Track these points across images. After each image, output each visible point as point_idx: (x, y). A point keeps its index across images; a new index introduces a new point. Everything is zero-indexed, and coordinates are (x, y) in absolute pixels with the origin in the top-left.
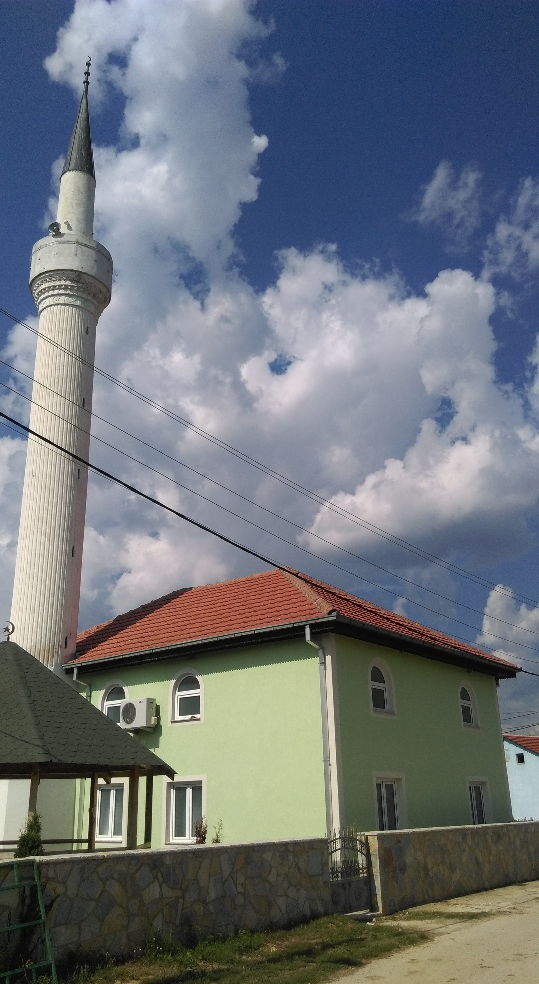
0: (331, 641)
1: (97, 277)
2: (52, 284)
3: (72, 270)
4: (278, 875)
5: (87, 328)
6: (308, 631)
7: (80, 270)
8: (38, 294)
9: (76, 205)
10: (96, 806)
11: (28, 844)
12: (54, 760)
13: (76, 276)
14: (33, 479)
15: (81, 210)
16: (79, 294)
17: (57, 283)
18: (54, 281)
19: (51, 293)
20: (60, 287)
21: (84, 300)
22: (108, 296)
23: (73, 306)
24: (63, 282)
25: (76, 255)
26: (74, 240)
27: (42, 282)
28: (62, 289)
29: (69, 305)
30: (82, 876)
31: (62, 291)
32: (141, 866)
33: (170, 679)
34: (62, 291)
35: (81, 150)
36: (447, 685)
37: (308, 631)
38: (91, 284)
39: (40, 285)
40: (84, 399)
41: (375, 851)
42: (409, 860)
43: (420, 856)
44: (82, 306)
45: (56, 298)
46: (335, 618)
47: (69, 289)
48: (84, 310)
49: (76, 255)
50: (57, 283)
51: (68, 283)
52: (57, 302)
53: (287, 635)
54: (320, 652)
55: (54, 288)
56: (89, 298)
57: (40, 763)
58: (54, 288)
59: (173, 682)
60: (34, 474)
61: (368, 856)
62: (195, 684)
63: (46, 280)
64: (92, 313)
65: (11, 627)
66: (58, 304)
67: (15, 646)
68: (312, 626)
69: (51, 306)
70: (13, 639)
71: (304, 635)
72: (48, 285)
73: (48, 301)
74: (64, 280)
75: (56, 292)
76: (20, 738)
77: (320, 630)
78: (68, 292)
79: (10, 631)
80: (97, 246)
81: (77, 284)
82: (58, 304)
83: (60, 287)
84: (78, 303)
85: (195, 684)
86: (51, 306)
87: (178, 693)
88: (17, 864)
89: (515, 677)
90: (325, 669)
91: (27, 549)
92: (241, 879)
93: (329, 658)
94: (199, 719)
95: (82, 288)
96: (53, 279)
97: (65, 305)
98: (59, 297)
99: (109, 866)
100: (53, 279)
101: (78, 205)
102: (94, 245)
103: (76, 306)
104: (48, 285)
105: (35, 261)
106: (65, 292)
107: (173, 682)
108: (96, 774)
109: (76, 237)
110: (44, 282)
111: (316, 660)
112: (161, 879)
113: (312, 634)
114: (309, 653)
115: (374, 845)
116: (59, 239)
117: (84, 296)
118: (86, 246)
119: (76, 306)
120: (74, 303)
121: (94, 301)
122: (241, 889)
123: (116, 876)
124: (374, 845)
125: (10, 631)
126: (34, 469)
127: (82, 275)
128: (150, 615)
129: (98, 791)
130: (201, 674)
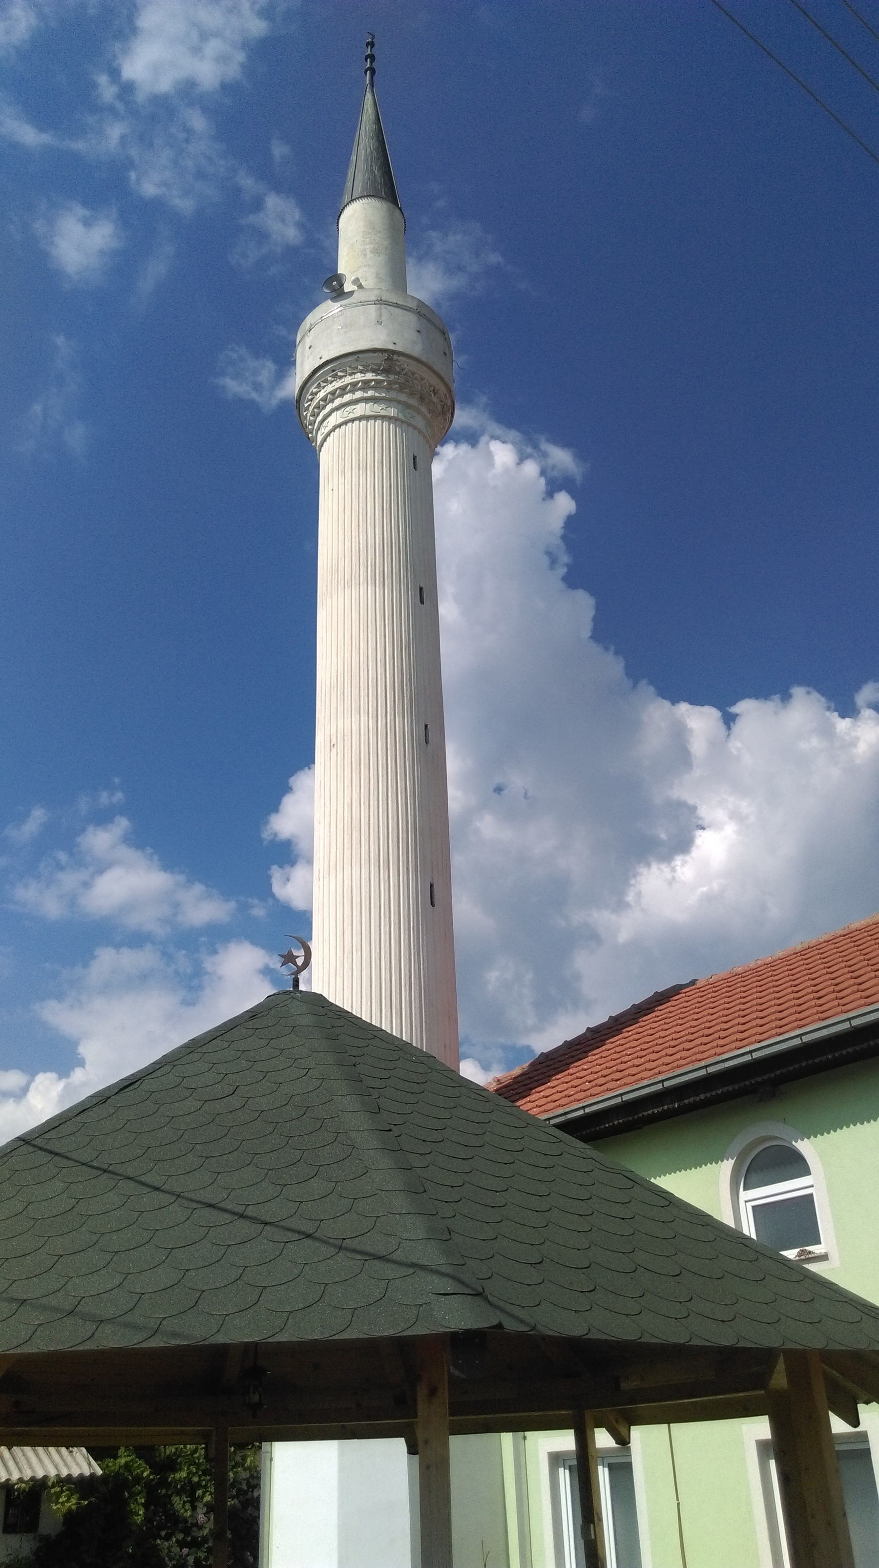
1: (424, 359)
2: (338, 384)
3: (375, 350)
5: (415, 458)
7: (391, 347)
8: (313, 415)
9: (372, 252)
10: (600, 1520)
12: (511, 1325)
13: (385, 361)
14: (334, 750)
15: (381, 259)
16: (393, 395)
17: (348, 380)
18: (341, 377)
19: (338, 402)
20: (354, 387)
21: (406, 406)
22: (449, 403)
23: (383, 418)
24: (359, 377)
25: (379, 323)
26: (374, 298)
27: (319, 386)
28: (357, 390)
29: (375, 417)
31: (359, 394)
33: (718, 1158)
34: (359, 394)
35: (371, 166)
38: (413, 374)
39: (316, 394)
40: (421, 589)
44: (401, 416)
45: (349, 408)
47: (373, 388)
48: (404, 426)
49: (379, 323)
50: (348, 380)
51: (370, 376)
52: (352, 416)
55: (343, 390)
56: (413, 402)
58: (343, 390)
59: (727, 1165)
60: (334, 741)
62: (796, 1165)
63: (326, 381)
64: (420, 431)
65: (300, 953)
66: (352, 420)
69: (340, 426)
72: (330, 388)
73: (333, 420)
74: (361, 372)
75: (348, 397)
78: (370, 393)
79: (300, 961)
80: (418, 306)
81: (387, 376)
82: (352, 420)
83: (354, 387)
84: (392, 412)
85: (796, 1165)
86: (340, 426)
87: (744, 1195)
94: (824, 1257)
95: (395, 383)
96: (340, 374)
97: (367, 418)
98: (353, 407)
100: (340, 374)
101: (375, 251)
102: (414, 305)
103: (389, 419)
104: (330, 388)
105: (303, 354)
106: (365, 395)
107: (727, 1165)
108: (588, 1415)
109: (376, 292)
110: (323, 384)
116: (344, 302)
117: (403, 397)
118: (396, 305)
119: (389, 419)
120: (383, 413)
121: (423, 409)
125: (300, 961)
126: (333, 731)
127: (395, 357)
128: (542, 1088)
129: (600, 1468)
130: (807, 1133)
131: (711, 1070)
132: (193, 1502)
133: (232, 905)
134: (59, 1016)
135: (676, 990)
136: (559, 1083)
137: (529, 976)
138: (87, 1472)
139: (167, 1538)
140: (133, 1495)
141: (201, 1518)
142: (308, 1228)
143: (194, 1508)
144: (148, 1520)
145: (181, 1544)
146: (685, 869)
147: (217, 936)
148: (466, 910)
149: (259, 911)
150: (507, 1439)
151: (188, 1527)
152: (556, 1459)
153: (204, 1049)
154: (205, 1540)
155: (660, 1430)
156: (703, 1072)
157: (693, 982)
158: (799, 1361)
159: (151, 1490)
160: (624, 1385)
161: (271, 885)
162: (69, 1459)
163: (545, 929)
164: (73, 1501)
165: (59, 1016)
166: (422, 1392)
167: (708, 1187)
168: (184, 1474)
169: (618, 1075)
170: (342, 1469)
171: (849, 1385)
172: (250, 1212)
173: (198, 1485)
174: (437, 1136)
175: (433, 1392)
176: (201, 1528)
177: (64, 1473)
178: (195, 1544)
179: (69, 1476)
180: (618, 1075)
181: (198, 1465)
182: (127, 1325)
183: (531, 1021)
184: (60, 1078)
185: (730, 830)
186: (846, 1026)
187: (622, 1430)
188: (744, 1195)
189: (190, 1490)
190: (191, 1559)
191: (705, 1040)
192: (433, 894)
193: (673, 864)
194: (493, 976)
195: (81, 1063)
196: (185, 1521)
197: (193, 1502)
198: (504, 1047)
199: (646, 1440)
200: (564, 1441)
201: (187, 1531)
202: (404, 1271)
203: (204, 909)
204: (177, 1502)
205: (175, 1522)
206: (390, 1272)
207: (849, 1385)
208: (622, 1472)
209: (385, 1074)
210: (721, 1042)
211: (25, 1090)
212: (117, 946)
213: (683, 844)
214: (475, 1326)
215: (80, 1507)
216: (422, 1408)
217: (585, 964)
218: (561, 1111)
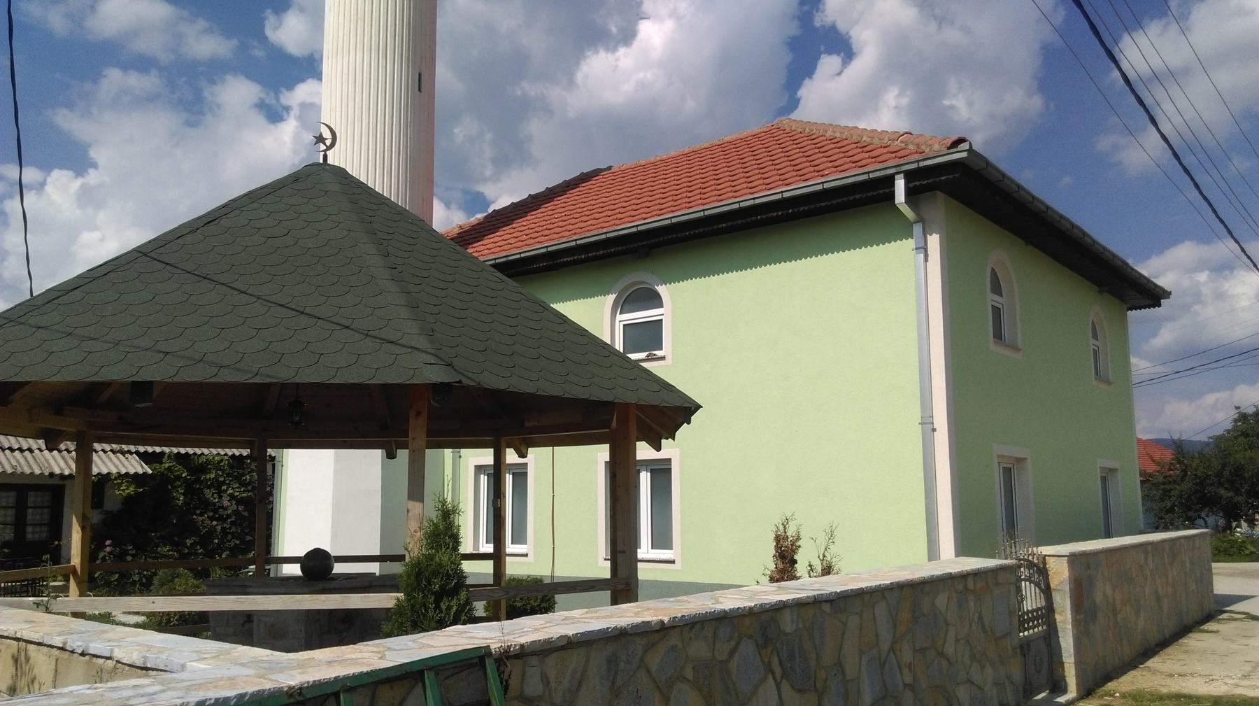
0: (939, 206)
4: (957, 640)
6: (900, 185)
11: (429, 583)
12: (466, 381)
30: (613, 683)
32: (738, 643)
36: (1086, 306)
37: (900, 185)
41: (1061, 583)
42: (1099, 598)
43: (1109, 590)
46: (964, 155)
53: (851, 198)
54: (917, 229)
57: (434, 385)
59: (611, 298)
61: (1047, 592)
62: (654, 300)
65: (327, 134)
67: (341, 173)
68: (909, 176)
70: (335, 158)
71: (892, 196)
76: (376, 333)
77: (926, 182)
85: (654, 300)
87: (619, 317)
88: (431, 669)
89: (1159, 305)
90: (926, 260)
91: (339, 75)
92: (907, 655)
93: (934, 241)
94: (663, 358)
99: (674, 648)
107: (611, 298)
108: (503, 440)
111: (909, 244)
112: (778, 670)
113: (910, 193)
114: (902, 230)
115: (1060, 573)
122: (908, 679)
123: (689, 674)
124: (1060, 573)
125: (328, 142)
130: (665, 282)
131: (609, 235)
132: (220, 493)
133: (235, 42)
134: (68, 121)
135: (596, 173)
136: (504, 233)
137: (489, 136)
138: (141, 471)
139: (201, 515)
140: (175, 488)
141: (226, 503)
142: (347, 323)
143: (221, 497)
144: (186, 503)
145: (212, 519)
146: (625, 57)
147: (216, 70)
148: (444, 76)
149: (258, 53)
150: (448, 453)
151: (216, 508)
152: (479, 469)
153: (262, 201)
154: (229, 516)
155: (546, 451)
156: (603, 237)
157: (610, 168)
158: (624, 409)
159: (189, 486)
160: (527, 424)
161: (263, 27)
162: (126, 463)
163: (507, 96)
164: (131, 489)
165: (68, 121)
166: (412, 413)
167: (595, 313)
168: (213, 476)
169: (547, 232)
170: (336, 472)
171: (657, 428)
172: (307, 311)
173: (223, 483)
174: (426, 274)
175: (418, 414)
176: (226, 509)
177: (123, 471)
178: (221, 519)
179: (127, 474)
180: (547, 232)
181: (223, 471)
182: (238, 370)
183: (488, 172)
184: (76, 177)
185: (669, 25)
186: (701, 214)
187: (524, 450)
188: (619, 317)
189: (217, 486)
190: (219, 528)
191: (609, 213)
192: (420, 82)
193: (618, 54)
194: (459, 132)
195: (94, 165)
196: (214, 504)
197: (220, 493)
198: (465, 192)
199: (537, 458)
200: (486, 456)
201: (215, 511)
202: (405, 350)
203: (206, 44)
204: (208, 493)
205: (206, 505)
206: (397, 349)
207: (657, 428)
208: (521, 475)
209: (391, 231)
210: (620, 216)
211: (43, 184)
212: (125, 67)
213: (628, 36)
214: (446, 380)
215: (137, 494)
216: (412, 422)
217: (537, 129)
218: (504, 254)
